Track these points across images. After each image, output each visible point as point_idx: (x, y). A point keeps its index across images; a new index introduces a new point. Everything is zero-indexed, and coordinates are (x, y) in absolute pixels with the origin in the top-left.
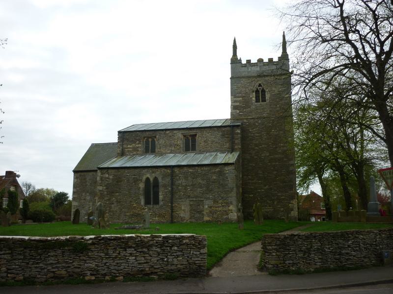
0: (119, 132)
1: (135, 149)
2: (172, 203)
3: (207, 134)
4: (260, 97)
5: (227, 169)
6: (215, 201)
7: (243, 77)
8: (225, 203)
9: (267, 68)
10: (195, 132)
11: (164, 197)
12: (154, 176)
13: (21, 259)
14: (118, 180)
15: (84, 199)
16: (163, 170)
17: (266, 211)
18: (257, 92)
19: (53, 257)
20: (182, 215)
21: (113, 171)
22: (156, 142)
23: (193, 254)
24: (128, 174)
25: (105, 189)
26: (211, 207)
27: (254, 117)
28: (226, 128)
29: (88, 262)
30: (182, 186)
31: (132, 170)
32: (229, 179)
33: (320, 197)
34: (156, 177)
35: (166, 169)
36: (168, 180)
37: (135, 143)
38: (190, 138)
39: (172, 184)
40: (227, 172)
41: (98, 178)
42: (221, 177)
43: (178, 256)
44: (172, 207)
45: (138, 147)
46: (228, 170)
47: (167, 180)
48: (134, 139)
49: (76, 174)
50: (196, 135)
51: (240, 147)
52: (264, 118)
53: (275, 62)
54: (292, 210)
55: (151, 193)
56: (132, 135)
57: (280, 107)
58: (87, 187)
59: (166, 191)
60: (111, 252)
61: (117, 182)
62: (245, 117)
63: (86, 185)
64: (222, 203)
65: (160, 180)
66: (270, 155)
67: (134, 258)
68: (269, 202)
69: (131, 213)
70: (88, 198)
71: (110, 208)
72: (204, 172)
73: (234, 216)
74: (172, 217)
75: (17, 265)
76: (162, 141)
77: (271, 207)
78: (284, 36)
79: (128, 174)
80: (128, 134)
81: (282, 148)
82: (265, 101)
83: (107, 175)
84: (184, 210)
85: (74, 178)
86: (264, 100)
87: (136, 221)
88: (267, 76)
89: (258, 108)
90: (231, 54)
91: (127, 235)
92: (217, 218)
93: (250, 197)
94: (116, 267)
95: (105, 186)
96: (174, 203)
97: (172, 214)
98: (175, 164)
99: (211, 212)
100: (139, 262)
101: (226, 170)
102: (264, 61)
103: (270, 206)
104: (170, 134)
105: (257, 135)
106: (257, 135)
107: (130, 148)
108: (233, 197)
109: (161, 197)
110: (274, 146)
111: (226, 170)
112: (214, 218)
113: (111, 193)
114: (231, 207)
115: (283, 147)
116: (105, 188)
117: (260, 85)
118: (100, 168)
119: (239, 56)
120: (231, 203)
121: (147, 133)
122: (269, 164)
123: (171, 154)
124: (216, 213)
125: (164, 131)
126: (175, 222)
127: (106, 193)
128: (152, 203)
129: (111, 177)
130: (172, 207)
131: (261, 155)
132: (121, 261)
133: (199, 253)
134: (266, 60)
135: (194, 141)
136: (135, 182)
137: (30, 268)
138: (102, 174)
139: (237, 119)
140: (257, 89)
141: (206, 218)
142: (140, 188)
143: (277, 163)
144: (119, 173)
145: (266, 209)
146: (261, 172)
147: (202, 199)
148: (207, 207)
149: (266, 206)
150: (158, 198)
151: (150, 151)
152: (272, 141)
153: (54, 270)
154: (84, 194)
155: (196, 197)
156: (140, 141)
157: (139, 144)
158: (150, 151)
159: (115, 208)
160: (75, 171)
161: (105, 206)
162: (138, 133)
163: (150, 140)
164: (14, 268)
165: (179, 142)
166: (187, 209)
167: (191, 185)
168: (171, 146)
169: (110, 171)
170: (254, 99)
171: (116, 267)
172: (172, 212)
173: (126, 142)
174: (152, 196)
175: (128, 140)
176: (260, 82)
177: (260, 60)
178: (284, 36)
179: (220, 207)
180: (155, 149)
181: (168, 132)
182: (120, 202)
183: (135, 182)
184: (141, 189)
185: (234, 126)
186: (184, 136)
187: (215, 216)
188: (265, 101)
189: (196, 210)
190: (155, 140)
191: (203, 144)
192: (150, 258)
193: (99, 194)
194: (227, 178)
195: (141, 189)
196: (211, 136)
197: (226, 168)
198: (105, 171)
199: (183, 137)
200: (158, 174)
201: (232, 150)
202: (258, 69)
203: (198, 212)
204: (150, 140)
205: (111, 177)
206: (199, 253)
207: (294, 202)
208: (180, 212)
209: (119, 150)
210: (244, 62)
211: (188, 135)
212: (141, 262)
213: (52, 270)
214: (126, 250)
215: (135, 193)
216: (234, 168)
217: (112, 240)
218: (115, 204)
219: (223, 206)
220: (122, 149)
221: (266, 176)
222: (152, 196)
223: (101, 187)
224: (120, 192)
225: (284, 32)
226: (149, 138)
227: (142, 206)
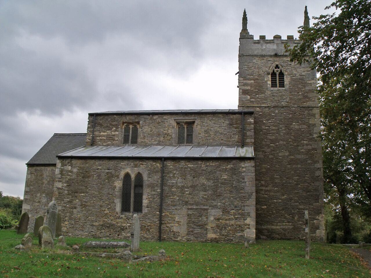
1: (111, 138)
2: (161, 211)
3: (208, 121)
5: (243, 166)
6: (225, 211)
7: (256, 56)
8: (239, 214)
10: (193, 118)
11: (150, 202)
12: (137, 172)
14: (85, 175)
15: (39, 202)
16: (150, 163)
17: (283, 229)
18: (273, 74)
20: (175, 229)
21: (79, 162)
22: (139, 130)
24: (99, 167)
25: (66, 187)
26: (218, 219)
27: (269, 105)
28: (234, 116)
30: (178, 187)
31: (106, 162)
32: (246, 180)
34: (139, 173)
35: (154, 162)
36: (157, 177)
37: (110, 129)
38: (185, 126)
39: (163, 184)
40: (244, 169)
42: (234, 176)
44: (161, 216)
45: (114, 135)
46: (245, 167)
47: (156, 177)
49: (30, 168)
50: (194, 122)
51: (253, 140)
52: (283, 107)
53: (267, 40)
54: (318, 228)
55: (131, 196)
56: (107, 120)
57: (303, 95)
58: (44, 185)
59: (153, 193)
61: (83, 177)
62: (258, 104)
63: (42, 184)
64: (235, 214)
65: (145, 177)
66: (290, 155)
69: (101, 223)
71: (72, 213)
72: (209, 169)
73: (251, 233)
74: (160, 232)
76: (147, 129)
77: (290, 224)
78: (306, 13)
79: (99, 167)
80: (102, 117)
81: (305, 147)
82: (283, 86)
83: (70, 168)
84: (178, 222)
85: (27, 174)
86: (282, 85)
87: (108, 234)
89: (275, 94)
92: (227, 236)
93: (262, 209)
95: (67, 182)
96: (164, 211)
97: (160, 227)
98: (168, 156)
99: (218, 226)
101: (243, 168)
102: (282, 39)
103: (289, 222)
105: (274, 128)
106: (274, 128)
107: (104, 136)
108: (251, 208)
109: (145, 202)
110: (295, 144)
111: (243, 168)
112: (223, 235)
113: (74, 193)
115: (307, 145)
116: (65, 185)
117: (277, 67)
118: (60, 158)
119: (251, 30)
120: (249, 215)
121: (128, 117)
122: (289, 166)
123: (159, 146)
124: (225, 228)
125: (151, 116)
126: (164, 239)
127: (66, 192)
128: (132, 210)
129: (75, 170)
130: (161, 216)
131: (278, 153)
134: (284, 38)
135: (135, 131)
136: (108, 178)
138: (63, 165)
139: (248, 107)
140: (274, 71)
141: (211, 235)
142: (115, 187)
143: (299, 166)
144: (87, 165)
145: (283, 225)
146: (278, 177)
147: (205, 207)
148: (212, 218)
149: (283, 222)
151: (130, 142)
152: (292, 137)
154: (38, 195)
155: (197, 204)
156: (117, 128)
157: (115, 131)
158: (130, 142)
159: (78, 213)
161: (64, 210)
162: (115, 116)
163: (131, 126)
165: (170, 132)
166: (184, 221)
167: (191, 187)
169: (74, 162)
170: (269, 83)
172: (161, 224)
173: (98, 128)
174: (132, 200)
175: (101, 125)
176: (277, 63)
177: (278, 37)
178: (306, 13)
179: (232, 219)
180: (137, 139)
181: (155, 117)
182: (85, 206)
183: (108, 178)
184: (117, 189)
186: (178, 123)
187: (224, 232)
188: (283, 86)
189: (196, 224)
190: (138, 126)
191: (203, 135)
193: (57, 193)
194: (244, 179)
195: (117, 189)
196: (215, 125)
197: (243, 164)
198: (67, 162)
199: (176, 124)
200: (143, 169)
201: (243, 144)
202: (275, 47)
203: (199, 226)
204: (131, 126)
205: (75, 170)
207: (320, 218)
208: (173, 225)
209: (88, 139)
210: (256, 38)
211: (183, 122)
215: (109, 194)
216: (254, 165)
218: (79, 209)
219: (236, 219)
220: (93, 137)
221: (284, 181)
222: (132, 200)
223: (61, 183)
224: (87, 193)
225: (306, 7)
226: (129, 123)
227: (117, 213)
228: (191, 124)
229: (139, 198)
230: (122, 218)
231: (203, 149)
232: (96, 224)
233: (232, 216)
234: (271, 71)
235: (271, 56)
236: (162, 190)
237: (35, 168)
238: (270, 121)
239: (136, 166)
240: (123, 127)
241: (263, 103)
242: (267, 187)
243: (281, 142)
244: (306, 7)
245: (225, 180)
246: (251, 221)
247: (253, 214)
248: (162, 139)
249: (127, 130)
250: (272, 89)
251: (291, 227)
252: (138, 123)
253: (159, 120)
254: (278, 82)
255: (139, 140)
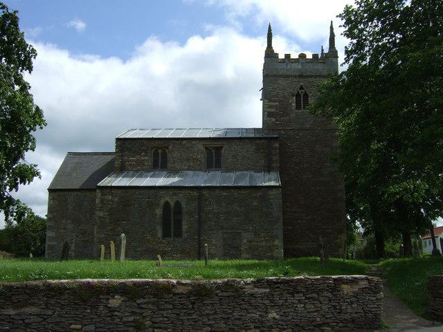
0: (118, 140)
1: (140, 163)
2: (199, 236)
4: (302, 101)
9: (284, 66)
13: (170, 309)
18: (298, 96)
19: (208, 305)
23: (369, 299)
26: (250, 242)
27: (294, 128)
29: (250, 311)
33: (43, 220)
41: (98, 201)
43: (352, 303)
46: (273, 195)
48: (137, 149)
49: (52, 194)
51: (278, 165)
53: (292, 59)
59: (192, 219)
60: (276, 298)
65: (183, 205)
67: (303, 305)
68: (312, 236)
70: (70, 227)
75: (166, 317)
76: (176, 154)
88: (311, 76)
90: (266, 46)
91: (296, 278)
94: (284, 318)
100: (308, 310)
102: (307, 57)
103: (313, 242)
104: (189, 145)
108: (279, 230)
109: (185, 227)
114: (276, 242)
117: (302, 88)
122: (313, 188)
128: (172, 236)
132: (289, 310)
133: (375, 299)
135: (164, 156)
137: (182, 320)
147: (239, 231)
148: (245, 241)
150: (181, 228)
153: (211, 322)
154: (64, 221)
157: (144, 156)
160: (50, 190)
163: (160, 151)
164: (161, 321)
168: (188, 160)
169: (114, 191)
170: (294, 104)
171: (284, 318)
172: (199, 247)
181: (184, 142)
184: (158, 217)
185: (272, 138)
186: (207, 148)
190: (167, 151)
192: (319, 305)
195: (158, 217)
200: (181, 196)
202: (300, 67)
206: (375, 299)
210: (282, 56)
212: (310, 310)
213: (208, 323)
214: (293, 296)
217: (278, 283)
219: (266, 240)
225: (332, 22)
226: (158, 148)
228: (219, 149)
229: (178, 223)
230: (163, 243)
231: (233, 175)
232: (140, 249)
233: (263, 239)
234: (295, 93)
235: (295, 77)
236: (200, 217)
237: (57, 193)
238: (375, 306)
239: (175, 194)
240: (152, 152)
241: (289, 126)
242: (292, 208)
243: (305, 165)
244: (332, 22)
245: (256, 206)
246: (278, 243)
247: (281, 236)
248: (192, 164)
249: (156, 154)
250: (296, 111)
251: (316, 246)
252: (167, 148)
253: (189, 145)
254: (302, 101)
255: (169, 165)
